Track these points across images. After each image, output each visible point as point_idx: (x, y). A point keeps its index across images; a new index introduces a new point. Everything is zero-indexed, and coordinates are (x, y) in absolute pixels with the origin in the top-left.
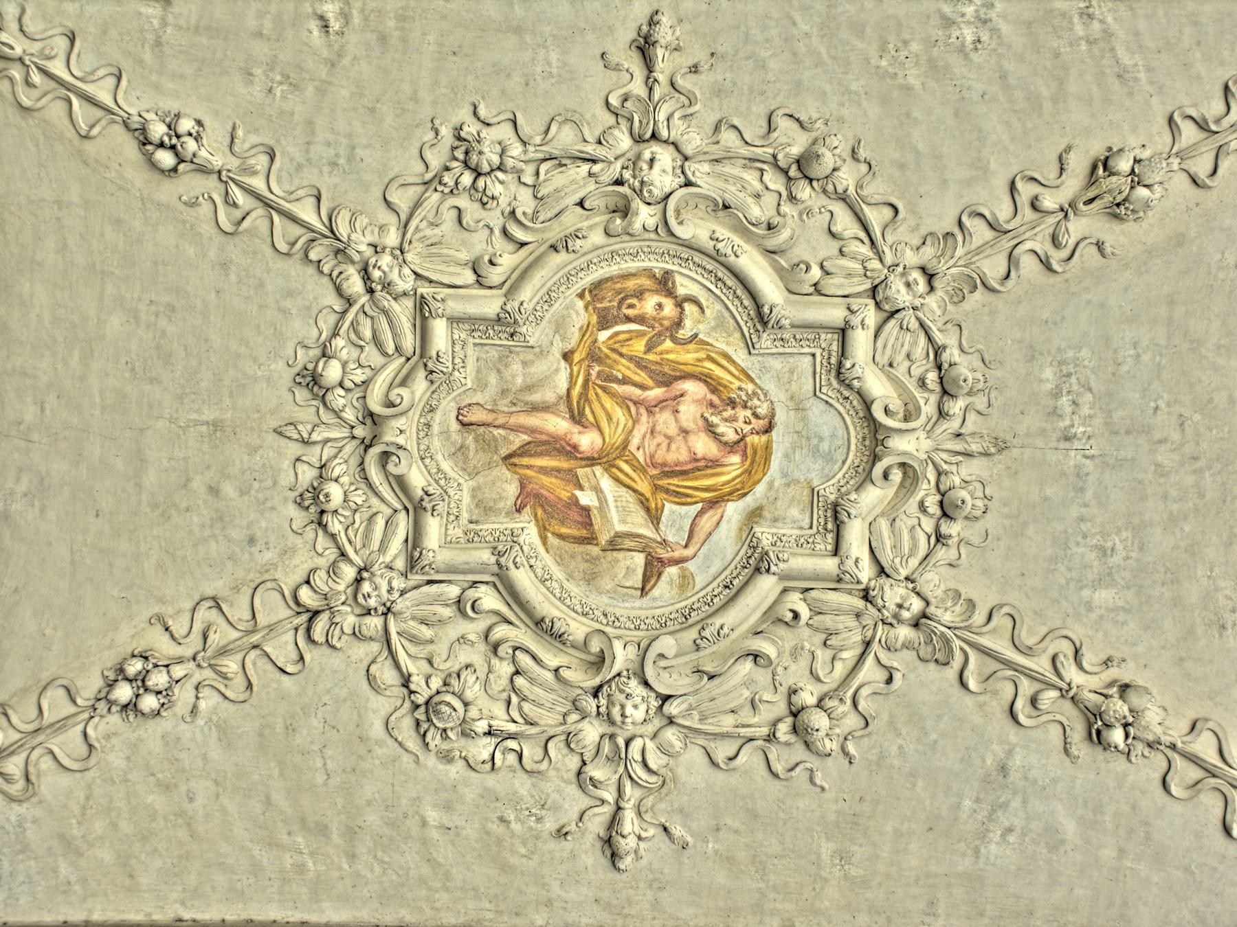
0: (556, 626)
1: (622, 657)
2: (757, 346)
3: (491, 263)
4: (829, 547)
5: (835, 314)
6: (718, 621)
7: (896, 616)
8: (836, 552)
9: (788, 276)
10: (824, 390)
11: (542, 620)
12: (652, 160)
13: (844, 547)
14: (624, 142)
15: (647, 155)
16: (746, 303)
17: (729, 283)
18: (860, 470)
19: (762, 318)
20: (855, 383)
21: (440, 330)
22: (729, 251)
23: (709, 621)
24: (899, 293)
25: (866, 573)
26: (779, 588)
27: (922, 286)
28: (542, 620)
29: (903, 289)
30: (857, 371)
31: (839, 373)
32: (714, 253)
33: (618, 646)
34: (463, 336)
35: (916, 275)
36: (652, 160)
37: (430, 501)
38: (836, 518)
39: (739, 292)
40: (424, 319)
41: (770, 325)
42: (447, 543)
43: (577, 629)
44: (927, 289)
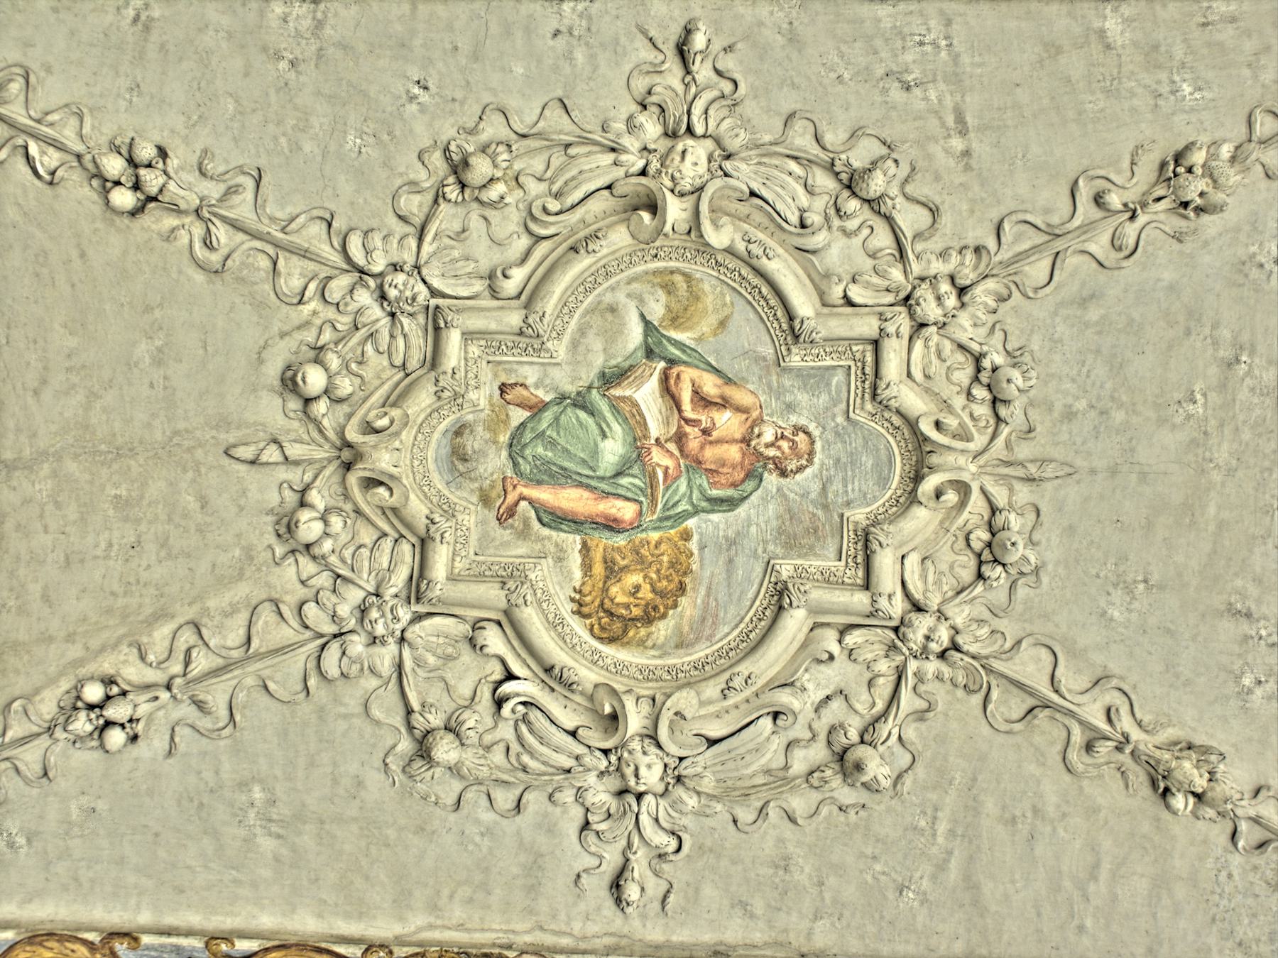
0: (565, 676)
1: (635, 721)
2: (787, 359)
3: (505, 276)
4: (859, 581)
5: (867, 326)
6: (744, 668)
7: (925, 649)
8: (867, 586)
9: (819, 283)
10: (857, 411)
11: (553, 667)
12: (684, 152)
13: (874, 580)
14: (651, 128)
15: (680, 147)
16: (772, 302)
17: (772, 302)
18: (901, 500)
19: (794, 332)
20: (893, 403)
21: (453, 339)
22: (761, 252)
23: (736, 670)
24: (930, 309)
25: (898, 607)
26: (810, 623)
27: (952, 301)
28: (553, 667)
29: (933, 304)
30: (893, 391)
31: (874, 396)
32: (747, 258)
33: (629, 703)
34: (477, 352)
35: (945, 287)
36: (684, 152)
37: (437, 530)
38: (866, 547)
39: (779, 314)
40: (437, 329)
41: (801, 340)
42: (452, 578)
43: (587, 676)
44: (958, 305)
